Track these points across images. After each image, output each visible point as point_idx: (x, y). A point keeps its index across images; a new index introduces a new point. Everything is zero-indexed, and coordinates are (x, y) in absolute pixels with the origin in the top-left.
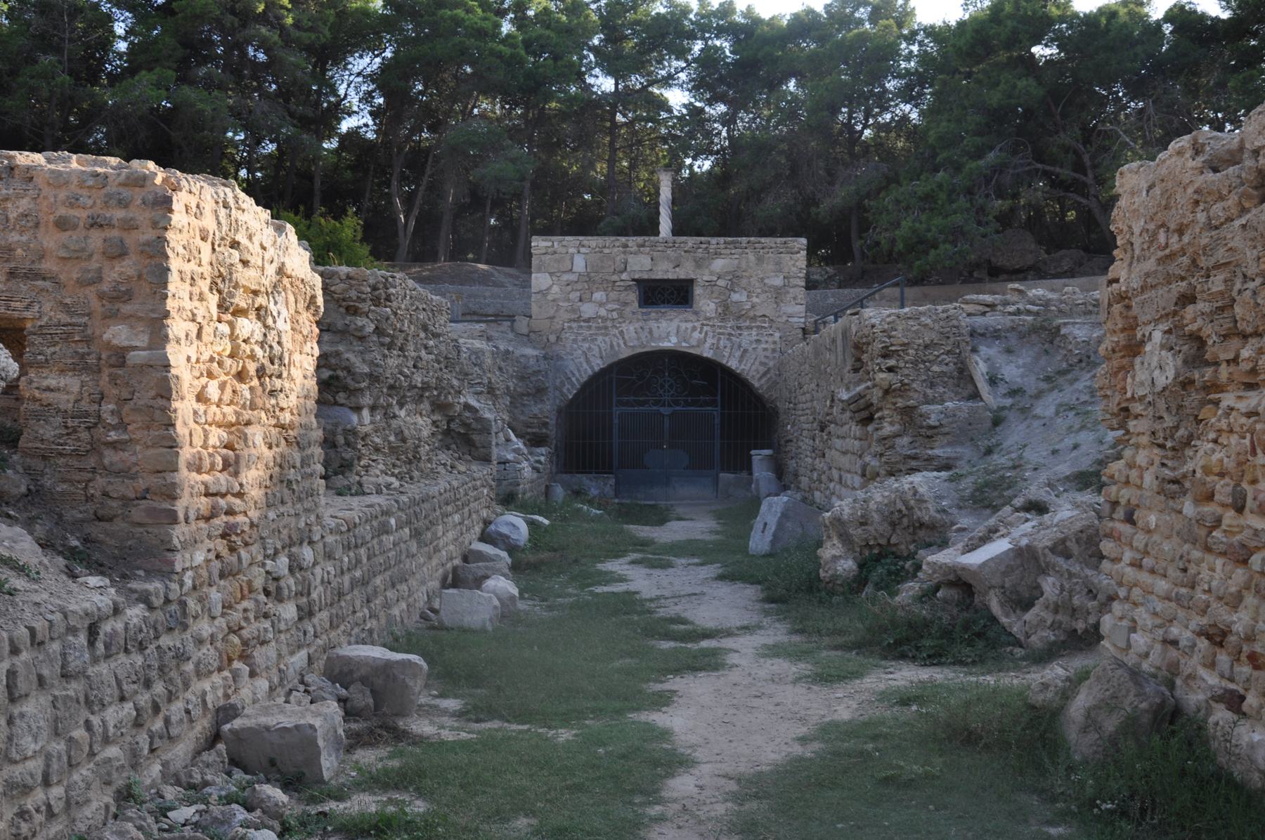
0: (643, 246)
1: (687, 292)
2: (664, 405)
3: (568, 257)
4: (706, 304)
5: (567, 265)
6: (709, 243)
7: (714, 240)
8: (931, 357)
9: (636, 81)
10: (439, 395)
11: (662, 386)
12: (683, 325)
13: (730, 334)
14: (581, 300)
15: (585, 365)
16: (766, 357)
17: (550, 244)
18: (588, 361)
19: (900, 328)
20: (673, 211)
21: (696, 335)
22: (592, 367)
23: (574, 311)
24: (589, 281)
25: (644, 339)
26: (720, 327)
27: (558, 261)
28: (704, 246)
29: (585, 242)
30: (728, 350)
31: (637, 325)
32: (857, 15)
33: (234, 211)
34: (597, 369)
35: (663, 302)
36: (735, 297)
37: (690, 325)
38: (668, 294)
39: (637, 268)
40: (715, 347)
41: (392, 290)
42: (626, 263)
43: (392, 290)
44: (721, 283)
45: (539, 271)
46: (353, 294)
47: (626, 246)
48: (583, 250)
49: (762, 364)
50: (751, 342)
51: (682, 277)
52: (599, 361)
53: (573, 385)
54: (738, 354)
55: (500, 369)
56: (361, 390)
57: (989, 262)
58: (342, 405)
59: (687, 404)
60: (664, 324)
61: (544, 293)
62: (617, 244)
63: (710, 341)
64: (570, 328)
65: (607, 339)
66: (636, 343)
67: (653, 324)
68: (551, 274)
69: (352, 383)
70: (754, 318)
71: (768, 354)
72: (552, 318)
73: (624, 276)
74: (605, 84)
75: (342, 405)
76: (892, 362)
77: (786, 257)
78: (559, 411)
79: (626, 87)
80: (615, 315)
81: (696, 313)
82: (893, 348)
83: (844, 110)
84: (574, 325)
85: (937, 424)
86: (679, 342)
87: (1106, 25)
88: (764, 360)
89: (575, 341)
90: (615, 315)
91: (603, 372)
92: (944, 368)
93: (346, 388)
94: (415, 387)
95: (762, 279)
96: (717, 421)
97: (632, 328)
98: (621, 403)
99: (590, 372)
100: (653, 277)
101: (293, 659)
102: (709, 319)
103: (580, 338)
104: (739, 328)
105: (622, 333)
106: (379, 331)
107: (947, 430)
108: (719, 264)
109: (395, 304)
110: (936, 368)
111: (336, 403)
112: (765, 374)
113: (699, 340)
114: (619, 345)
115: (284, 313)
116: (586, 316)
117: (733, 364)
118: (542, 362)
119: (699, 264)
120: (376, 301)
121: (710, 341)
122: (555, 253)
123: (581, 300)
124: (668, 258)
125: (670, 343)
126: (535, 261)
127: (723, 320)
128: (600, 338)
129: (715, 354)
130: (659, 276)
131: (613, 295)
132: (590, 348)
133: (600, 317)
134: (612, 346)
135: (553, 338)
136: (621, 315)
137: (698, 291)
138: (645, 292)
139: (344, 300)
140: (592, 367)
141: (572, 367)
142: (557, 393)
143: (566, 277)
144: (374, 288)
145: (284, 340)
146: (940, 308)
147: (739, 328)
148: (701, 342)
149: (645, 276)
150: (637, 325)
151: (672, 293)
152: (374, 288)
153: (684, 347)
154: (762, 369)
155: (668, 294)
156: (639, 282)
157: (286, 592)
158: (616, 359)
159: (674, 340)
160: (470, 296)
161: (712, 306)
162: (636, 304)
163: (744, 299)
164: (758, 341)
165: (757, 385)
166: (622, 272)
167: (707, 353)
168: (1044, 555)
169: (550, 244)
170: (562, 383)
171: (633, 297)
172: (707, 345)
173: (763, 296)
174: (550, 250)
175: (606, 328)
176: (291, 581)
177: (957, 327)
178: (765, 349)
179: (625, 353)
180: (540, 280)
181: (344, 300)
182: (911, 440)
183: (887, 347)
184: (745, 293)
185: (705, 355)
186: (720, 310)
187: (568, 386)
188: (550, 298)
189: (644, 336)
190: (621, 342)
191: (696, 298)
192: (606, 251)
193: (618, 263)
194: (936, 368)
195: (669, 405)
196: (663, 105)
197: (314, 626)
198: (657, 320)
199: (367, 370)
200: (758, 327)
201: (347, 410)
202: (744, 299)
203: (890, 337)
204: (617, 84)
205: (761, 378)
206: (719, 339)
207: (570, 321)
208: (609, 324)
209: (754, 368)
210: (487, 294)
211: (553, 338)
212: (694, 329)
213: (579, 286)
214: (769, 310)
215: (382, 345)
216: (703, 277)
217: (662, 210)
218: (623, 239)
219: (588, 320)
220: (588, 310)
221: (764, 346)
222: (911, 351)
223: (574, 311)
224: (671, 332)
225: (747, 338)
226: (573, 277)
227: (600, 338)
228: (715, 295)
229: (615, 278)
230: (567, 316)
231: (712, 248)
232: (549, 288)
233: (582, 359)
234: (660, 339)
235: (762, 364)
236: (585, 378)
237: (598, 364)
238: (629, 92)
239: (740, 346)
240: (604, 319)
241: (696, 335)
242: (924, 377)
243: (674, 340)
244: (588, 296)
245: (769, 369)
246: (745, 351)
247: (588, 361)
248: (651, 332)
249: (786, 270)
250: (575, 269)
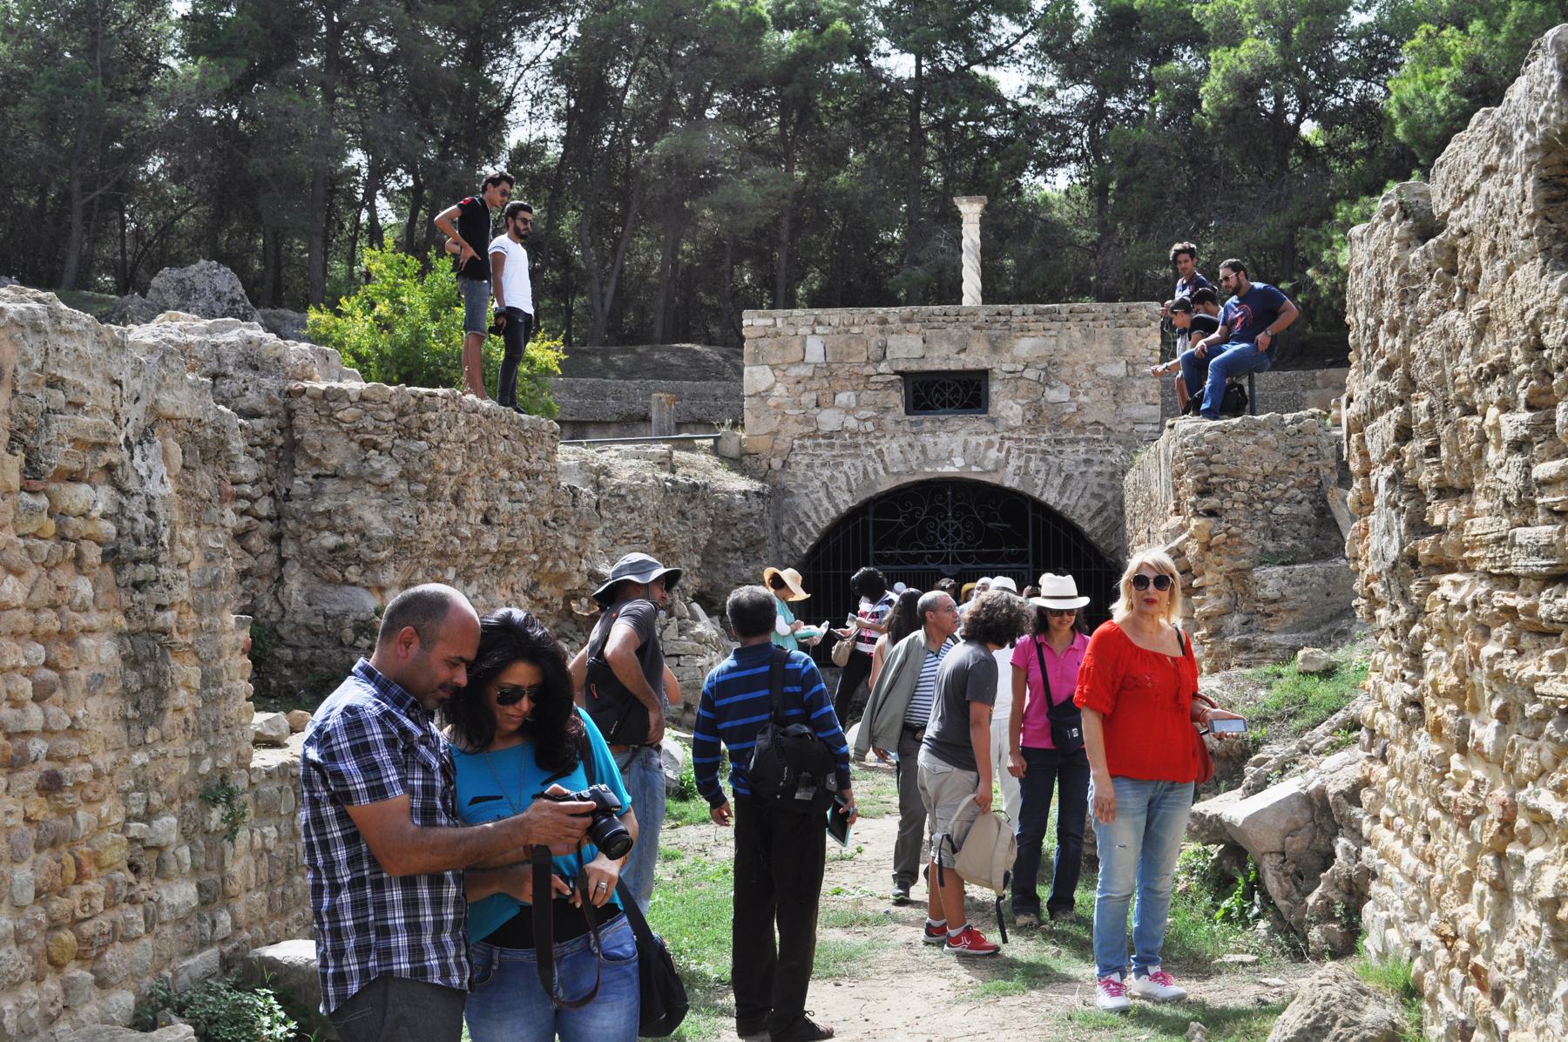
0: (909, 320)
1: (979, 388)
2: (946, 562)
3: (797, 341)
4: (1007, 406)
5: (795, 353)
6: (1010, 313)
7: (1017, 309)
8: (1275, 493)
9: (950, 59)
10: (543, 561)
11: (944, 533)
12: (973, 440)
13: (1045, 452)
14: (818, 405)
15: (826, 503)
16: (1100, 485)
17: (770, 322)
18: (830, 496)
19: (1226, 448)
20: (982, 265)
21: (993, 454)
22: (836, 506)
23: (807, 421)
24: (829, 374)
25: (914, 463)
26: (1030, 441)
27: (783, 346)
28: (1003, 319)
29: (824, 318)
30: (1042, 475)
31: (903, 441)
33: (52, 336)
34: (843, 508)
35: (943, 405)
36: (1052, 395)
37: (983, 439)
38: (949, 393)
39: (901, 354)
40: (1023, 472)
41: (431, 415)
42: (884, 348)
43: (431, 415)
44: (1031, 374)
45: (755, 362)
46: (368, 422)
47: (884, 321)
48: (819, 329)
49: (1094, 496)
50: (1077, 464)
51: (970, 366)
52: (847, 497)
53: (808, 533)
54: (1058, 481)
55: (682, 513)
56: (382, 563)
58: (354, 584)
60: (944, 438)
61: (763, 396)
62: (872, 319)
63: (1014, 463)
64: (802, 447)
65: (858, 463)
66: (902, 468)
67: (927, 439)
68: (773, 367)
69: (367, 551)
70: (1082, 427)
71: (1105, 480)
72: (777, 433)
73: (883, 368)
74: (901, 65)
75: (354, 584)
76: (1212, 502)
77: (1130, 332)
79: (934, 70)
80: (870, 426)
81: (993, 421)
82: (1214, 480)
84: (809, 443)
85: (1277, 595)
86: (968, 465)
88: (1097, 490)
89: (810, 466)
90: (870, 426)
91: (854, 513)
92: (1296, 510)
93: (358, 560)
94: (487, 552)
95: (1093, 367)
97: (895, 445)
99: (833, 513)
100: (928, 367)
101: (190, 962)
102: (1012, 429)
103: (817, 462)
104: (1059, 442)
105: (880, 453)
106: (408, 476)
107: (1292, 604)
108: (1025, 346)
109: (434, 436)
110: (1281, 509)
111: (346, 582)
112: (1100, 511)
113: (997, 462)
114: (876, 472)
115: (162, 470)
116: (826, 429)
117: (1050, 497)
118: (754, 501)
119: (995, 346)
120: (406, 433)
121: (1014, 463)
122: (778, 334)
123: (818, 405)
124: (949, 339)
125: (953, 468)
126: (748, 348)
127: (1034, 430)
128: (848, 462)
129: (1022, 482)
130: (935, 364)
131: (867, 396)
132: (832, 477)
133: (846, 430)
134: (866, 473)
135: (777, 463)
136: (879, 427)
137: (995, 388)
138: (915, 391)
139: (356, 431)
140: (836, 506)
141: (807, 506)
142: (784, 546)
143: (794, 372)
144: (402, 413)
145: (158, 508)
146: (1288, 417)
147: (1059, 442)
148: (1001, 465)
149: (915, 367)
150: (903, 441)
151: (956, 391)
152: (402, 413)
153: (975, 473)
154: (1096, 505)
156: (904, 375)
157: (173, 866)
158: (871, 494)
159: (959, 462)
160: (693, 396)
161: (1018, 409)
162: (902, 409)
163: (1065, 397)
164: (1088, 462)
165: (1087, 528)
166: (879, 362)
167: (1010, 481)
168: (1337, 804)
169: (770, 322)
170: (792, 531)
171: (896, 399)
172: (1010, 469)
173: (1095, 393)
174: (770, 331)
175: (857, 446)
176: (185, 851)
177: (1315, 446)
178: (1099, 474)
179: (886, 484)
180: (756, 377)
181: (356, 431)
182: (1244, 618)
183: (1206, 479)
184: (1067, 389)
185: (1007, 484)
186: (1029, 416)
187: (800, 535)
188: (771, 402)
189: (914, 457)
190: (880, 467)
191: (993, 397)
192: (855, 330)
193: (873, 347)
194: (1281, 509)
195: (955, 562)
196: (989, 92)
197: (233, 915)
198: (933, 432)
199: (388, 532)
200: (1087, 440)
201: (360, 590)
202: (1065, 397)
203: (1209, 463)
204: (919, 67)
205: (1093, 518)
206: (1028, 460)
207: (802, 437)
208: (861, 440)
209: (1082, 502)
210: (720, 392)
211: (777, 463)
212: (990, 444)
213: (815, 384)
214: (1103, 413)
215: (415, 495)
216: (1001, 366)
217: (965, 258)
218: (880, 311)
219: (829, 436)
220: (829, 419)
221: (1097, 468)
222: (1241, 484)
223: (807, 421)
224: (954, 450)
225: (1073, 455)
226: (806, 371)
227: (848, 462)
228: (1021, 392)
229: (869, 370)
230: (798, 429)
231: (1015, 322)
232: (769, 390)
233: (822, 494)
234: (938, 460)
235: (1094, 496)
236: (825, 522)
237: (846, 501)
238: (940, 74)
239: (1060, 470)
240: (854, 434)
241: (993, 454)
242: (1261, 524)
243: (959, 462)
244: (829, 398)
245: (1106, 504)
246: (1069, 477)
247: (830, 496)
248: (924, 451)
249: (1130, 352)
250: (807, 359)
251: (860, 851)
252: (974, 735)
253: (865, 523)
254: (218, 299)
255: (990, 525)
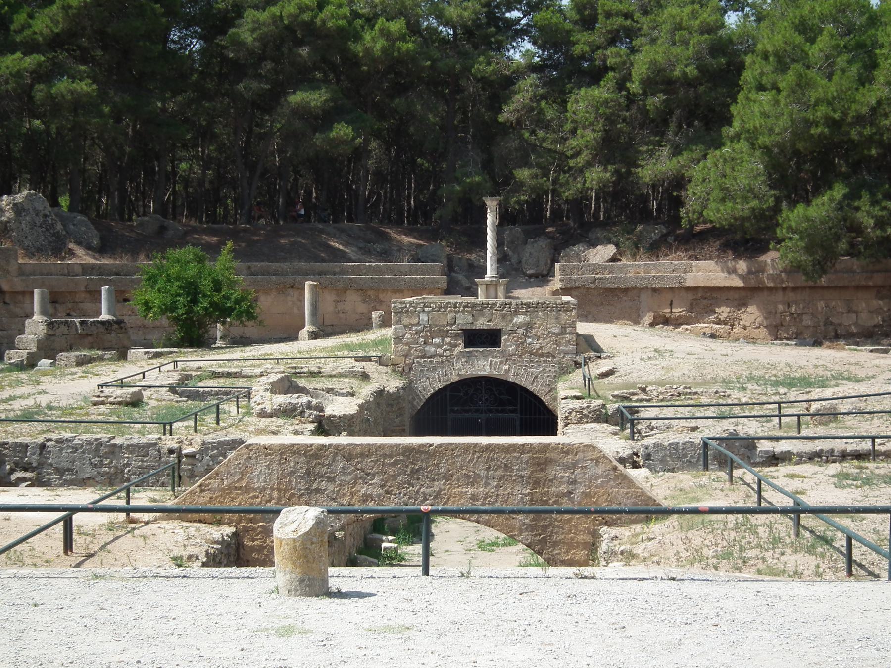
32: (501, 119)
38: (483, 339)
44: (520, 331)
48: (426, 309)
57: (11, 74)
59: (498, 411)
70: (542, 355)
78: (412, 417)
83: (175, 35)
87: (640, 151)
96: (518, 423)
98: (453, 411)
148: (507, 371)
151: (487, 338)
155: (483, 339)
156: (465, 331)
166: (453, 325)
170: (414, 399)
224: (485, 365)
230: (418, 354)
240: (441, 356)
251: (755, 102)
252: (842, 343)
253: (446, 395)
254: (37, 215)
255: (502, 397)
